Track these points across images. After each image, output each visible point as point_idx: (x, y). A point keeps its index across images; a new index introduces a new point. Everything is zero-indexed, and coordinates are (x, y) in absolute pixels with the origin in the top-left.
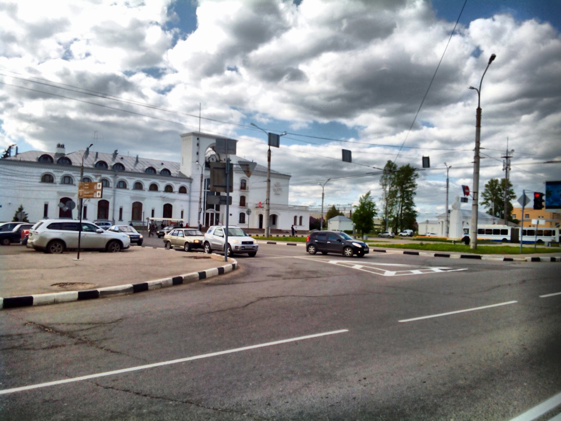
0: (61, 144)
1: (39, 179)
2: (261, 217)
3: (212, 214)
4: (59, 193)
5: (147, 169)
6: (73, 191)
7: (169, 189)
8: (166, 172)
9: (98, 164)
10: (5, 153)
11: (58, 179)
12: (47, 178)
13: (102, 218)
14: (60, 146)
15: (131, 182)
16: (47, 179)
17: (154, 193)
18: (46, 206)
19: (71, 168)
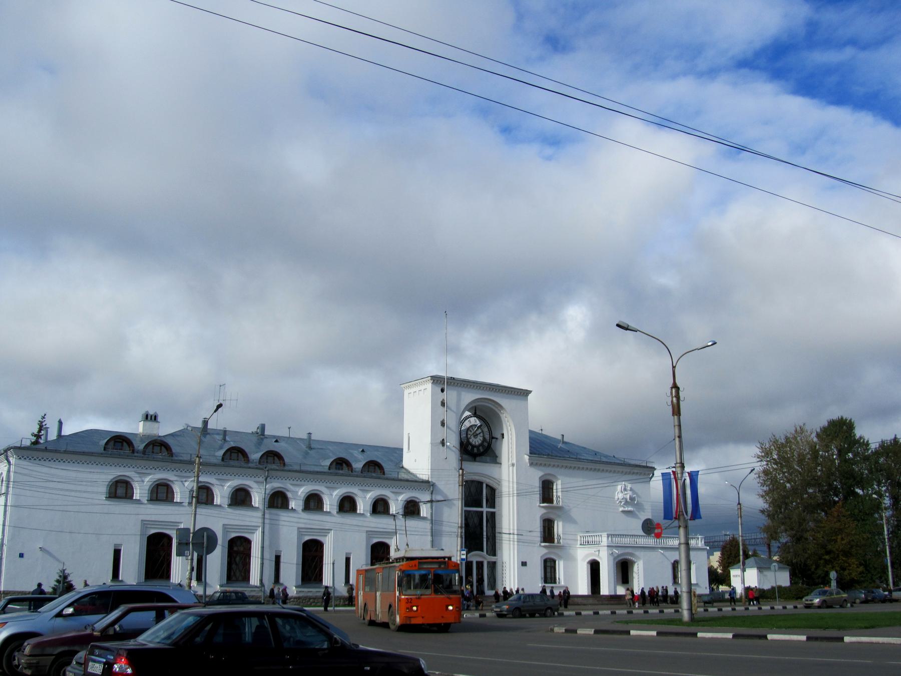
0: (151, 413)
1: (103, 489)
2: (594, 567)
3: (480, 565)
4: (145, 524)
5: (364, 465)
6: (178, 517)
7: (380, 507)
8: (273, 458)
9: (112, 443)
10: (34, 439)
11: (140, 491)
12: (162, 490)
13: (237, 580)
14: (150, 418)
15: (298, 493)
16: (120, 490)
17: (412, 523)
18: (117, 553)
19: (386, 482)
